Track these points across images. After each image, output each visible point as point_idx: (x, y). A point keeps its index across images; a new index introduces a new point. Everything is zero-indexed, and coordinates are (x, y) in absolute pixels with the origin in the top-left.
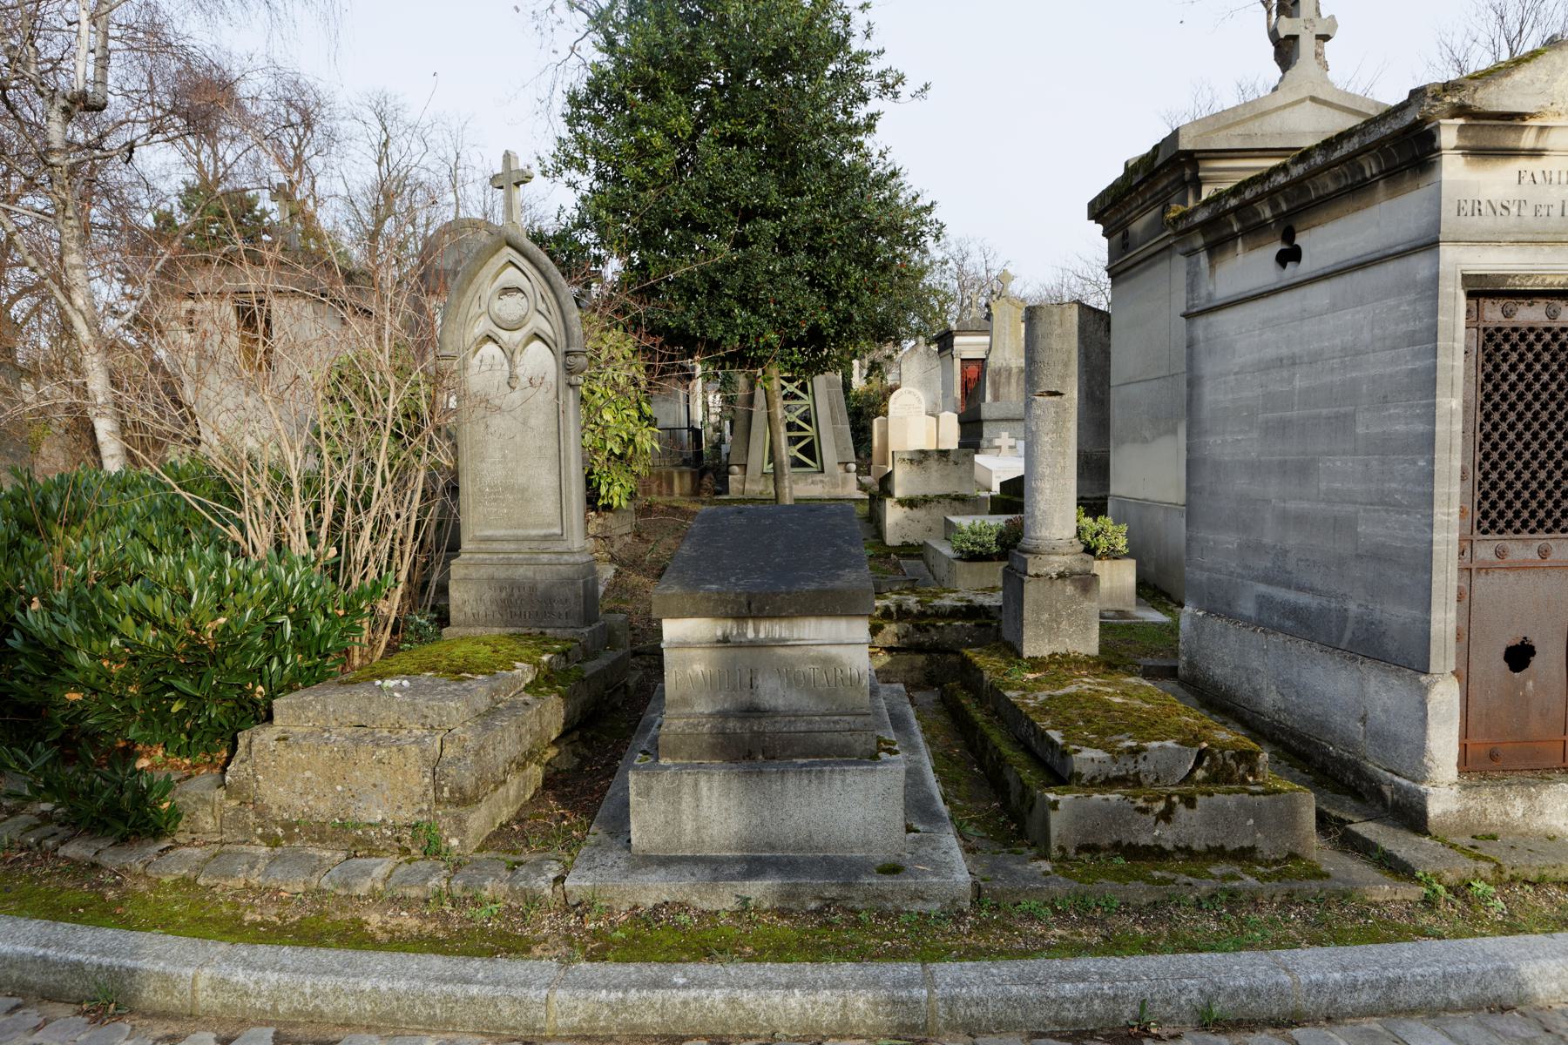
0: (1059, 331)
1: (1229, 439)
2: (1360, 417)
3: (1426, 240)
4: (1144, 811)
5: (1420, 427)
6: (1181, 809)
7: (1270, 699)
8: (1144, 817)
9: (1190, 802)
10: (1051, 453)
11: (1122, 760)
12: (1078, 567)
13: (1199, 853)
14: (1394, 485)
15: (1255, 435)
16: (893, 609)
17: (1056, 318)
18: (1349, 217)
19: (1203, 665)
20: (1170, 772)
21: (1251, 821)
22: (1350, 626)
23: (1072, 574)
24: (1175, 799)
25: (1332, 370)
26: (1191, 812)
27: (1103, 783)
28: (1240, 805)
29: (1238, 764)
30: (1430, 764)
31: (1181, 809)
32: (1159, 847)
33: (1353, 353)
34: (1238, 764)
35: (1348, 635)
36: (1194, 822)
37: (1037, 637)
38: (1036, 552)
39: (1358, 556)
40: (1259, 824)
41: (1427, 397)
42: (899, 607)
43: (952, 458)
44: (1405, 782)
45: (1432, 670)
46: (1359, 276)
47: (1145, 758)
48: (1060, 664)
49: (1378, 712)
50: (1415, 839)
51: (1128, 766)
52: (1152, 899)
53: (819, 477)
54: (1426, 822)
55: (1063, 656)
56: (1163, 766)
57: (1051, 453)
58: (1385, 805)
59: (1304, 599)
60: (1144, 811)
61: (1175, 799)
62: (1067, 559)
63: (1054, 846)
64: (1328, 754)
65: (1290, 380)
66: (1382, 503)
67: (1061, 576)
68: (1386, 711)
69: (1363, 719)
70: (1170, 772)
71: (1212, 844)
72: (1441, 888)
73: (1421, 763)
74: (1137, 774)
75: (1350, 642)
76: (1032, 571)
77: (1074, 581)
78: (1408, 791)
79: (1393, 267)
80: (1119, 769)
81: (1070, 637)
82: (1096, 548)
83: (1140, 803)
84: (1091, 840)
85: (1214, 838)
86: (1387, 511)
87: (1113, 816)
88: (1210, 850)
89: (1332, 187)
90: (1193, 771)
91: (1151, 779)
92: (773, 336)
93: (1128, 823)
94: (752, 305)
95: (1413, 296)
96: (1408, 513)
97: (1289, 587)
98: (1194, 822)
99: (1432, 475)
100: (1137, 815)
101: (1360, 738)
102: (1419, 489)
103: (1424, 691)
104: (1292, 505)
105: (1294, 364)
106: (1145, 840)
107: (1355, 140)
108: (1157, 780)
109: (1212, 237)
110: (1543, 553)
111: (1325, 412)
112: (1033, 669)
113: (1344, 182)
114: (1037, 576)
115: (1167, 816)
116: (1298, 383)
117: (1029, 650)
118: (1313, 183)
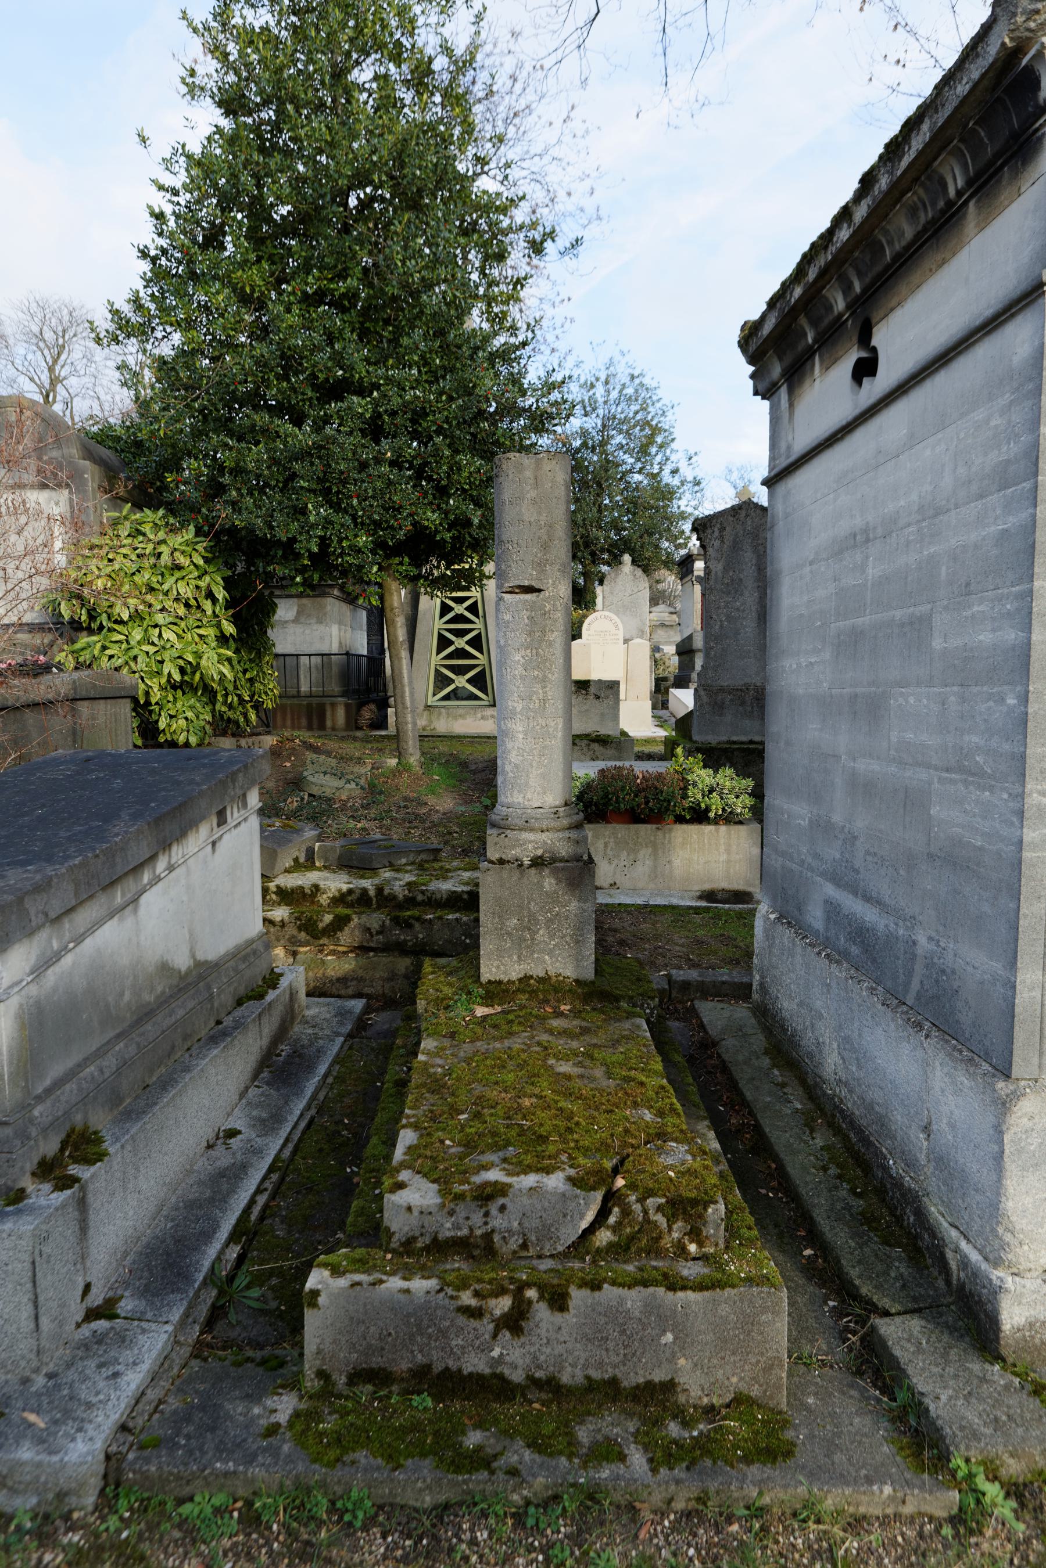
0: (533, 494)
1: (803, 662)
2: (937, 621)
3: (1024, 286)
4: (475, 1313)
5: (1011, 636)
6: (542, 1312)
7: (831, 1063)
8: (474, 1323)
9: (558, 1301)
10: (523, 678)
11: (461, 1210)
12: (564, 850)
13: (570, 1391)
14: (975, 739)
15: (827, 655)
16: (372, 893)
17: (528, 474)
18: (931, 282)
19: (773, 990)
20: (547, 1233)
21: (669, 1337)
22: (919, 969)
23: (554, 860)
24: (531, 1293)
25: (908, 543)
26: (558, 1318)
27: (427, 1249)
28: (650, 1307)
29: (671, 1221)
30: (1008, 1237)
31: (542, 1312)
32: (501, 1378)
33: (931, 512)
34: (671, 1221)
35: (915, 985)
36: (564, 1335)
37: (501, 952)
38: (502, 827)
39: (930, 856)
40: (682, 1341)
41: (1020, 581)
42: (380, 890)
43: (592, 690)
44: (974, 1256)
45: (1015, 1072)
46: (941, 380)
47: (503, 1208)
48: (533, 993)
49: (944, 1126)
50: (976, 1366)
51: (470, 1221)
52: (442, 1498)
53: (490, 711)
54: (997, 1339)
55: (541, 980)
56: (535, 1223)
57: (523, 678)
58: (948, 1282)
59: (869, 915)
60: (475, 1313)
61: (531, 1293)
62: (545, 837)
63: (309, 1367)
64: (886, 1169)
65: (863, 568)
66: (961, 769)
67: (538, 862)
68: (952, 1126)
69: (927, 1129)
70: (547, 1233)
71: (596, 1375)
72: (992, 1491)
73: (994, 1231)
74: (488, 1236)
75: (918, 997)
76: (493, 854)
77: (555, 872)
78: (976, 1274)
79: (983, 352)
80: (457, 1227)
81: (550, 953)
82: (708, 809)
83: (467, 1298)
84: (376, 1362)
85: (601, 1365)
86: (965, 782)
87: (417, 1319)
88: (591, 1386)
89: (909, 233)
90: (591, 1230)
91: (514, 1243)
92: (363, 540)
93: (444, 1333)
94: (329, 492)
95: (1008, 397)
96: (991, 789)
97: (855, 894)
98: (564, 1335)
99: (1023, 721)
100: (461, 1320)
101: (922, 1159)
102: (1006, 747)
103: (1004, 1106)
104: (862, 765)
105: (867, 540)
106: (474, 1364)
107: (925, 127)
108: (524, 1246)
109: (789, 359)
110: (783, 1085)
111: (898, 614)
112: (488, 999)
113: (923, 220)
114: (501, 862)
115: (515, 1322)
116: (873, 572)
117: (489, 971)
118: (886, 232)
